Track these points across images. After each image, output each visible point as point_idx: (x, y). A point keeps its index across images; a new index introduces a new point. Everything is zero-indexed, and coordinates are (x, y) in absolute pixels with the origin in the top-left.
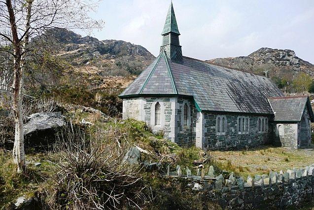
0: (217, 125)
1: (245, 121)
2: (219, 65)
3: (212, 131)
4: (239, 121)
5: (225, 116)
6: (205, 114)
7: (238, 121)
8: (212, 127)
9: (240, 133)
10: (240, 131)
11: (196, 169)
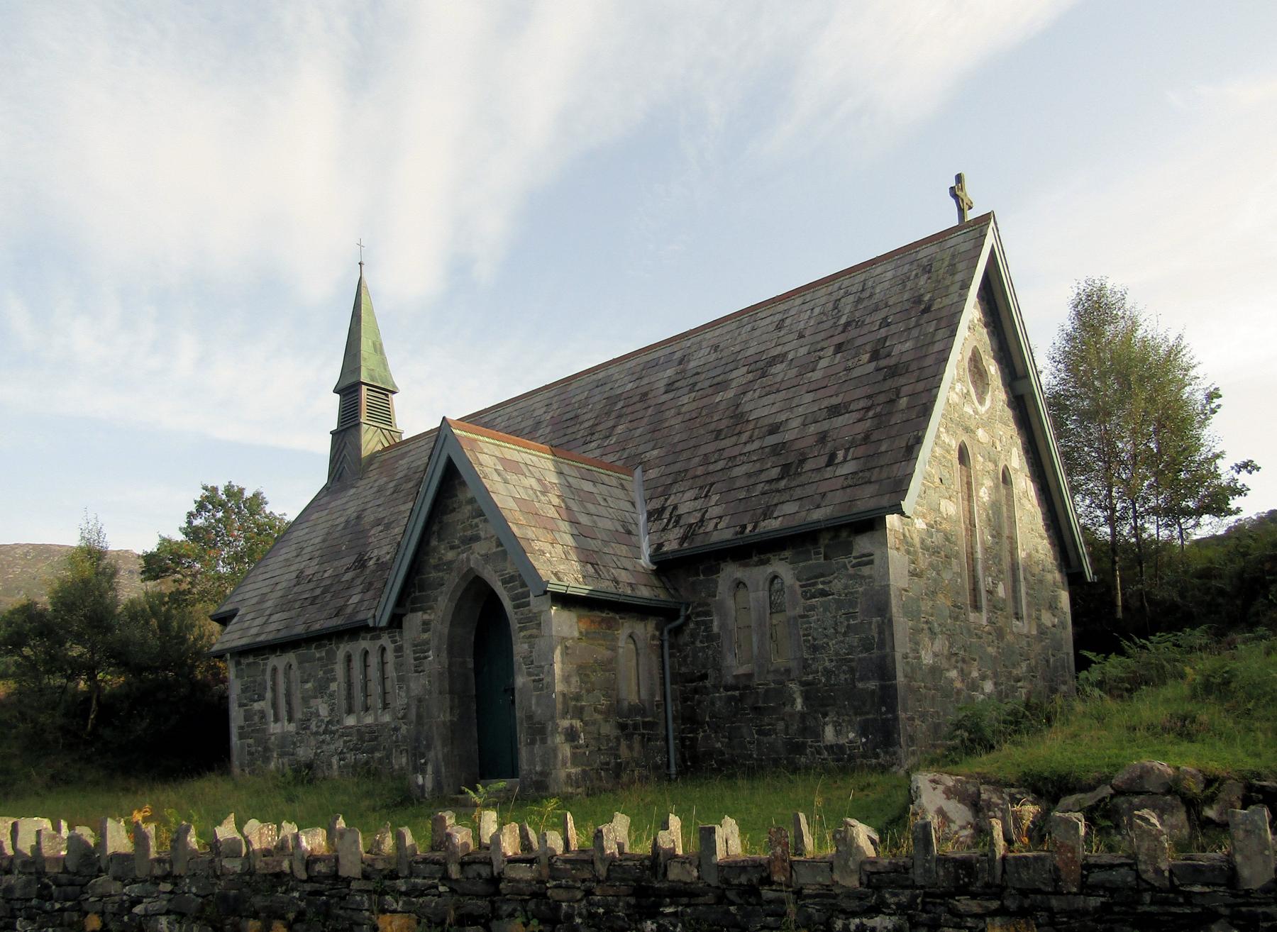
0: (269, 695)
5: (291, 657)
6: (238, 664)
7: (339, 669)
10: (350, 711)
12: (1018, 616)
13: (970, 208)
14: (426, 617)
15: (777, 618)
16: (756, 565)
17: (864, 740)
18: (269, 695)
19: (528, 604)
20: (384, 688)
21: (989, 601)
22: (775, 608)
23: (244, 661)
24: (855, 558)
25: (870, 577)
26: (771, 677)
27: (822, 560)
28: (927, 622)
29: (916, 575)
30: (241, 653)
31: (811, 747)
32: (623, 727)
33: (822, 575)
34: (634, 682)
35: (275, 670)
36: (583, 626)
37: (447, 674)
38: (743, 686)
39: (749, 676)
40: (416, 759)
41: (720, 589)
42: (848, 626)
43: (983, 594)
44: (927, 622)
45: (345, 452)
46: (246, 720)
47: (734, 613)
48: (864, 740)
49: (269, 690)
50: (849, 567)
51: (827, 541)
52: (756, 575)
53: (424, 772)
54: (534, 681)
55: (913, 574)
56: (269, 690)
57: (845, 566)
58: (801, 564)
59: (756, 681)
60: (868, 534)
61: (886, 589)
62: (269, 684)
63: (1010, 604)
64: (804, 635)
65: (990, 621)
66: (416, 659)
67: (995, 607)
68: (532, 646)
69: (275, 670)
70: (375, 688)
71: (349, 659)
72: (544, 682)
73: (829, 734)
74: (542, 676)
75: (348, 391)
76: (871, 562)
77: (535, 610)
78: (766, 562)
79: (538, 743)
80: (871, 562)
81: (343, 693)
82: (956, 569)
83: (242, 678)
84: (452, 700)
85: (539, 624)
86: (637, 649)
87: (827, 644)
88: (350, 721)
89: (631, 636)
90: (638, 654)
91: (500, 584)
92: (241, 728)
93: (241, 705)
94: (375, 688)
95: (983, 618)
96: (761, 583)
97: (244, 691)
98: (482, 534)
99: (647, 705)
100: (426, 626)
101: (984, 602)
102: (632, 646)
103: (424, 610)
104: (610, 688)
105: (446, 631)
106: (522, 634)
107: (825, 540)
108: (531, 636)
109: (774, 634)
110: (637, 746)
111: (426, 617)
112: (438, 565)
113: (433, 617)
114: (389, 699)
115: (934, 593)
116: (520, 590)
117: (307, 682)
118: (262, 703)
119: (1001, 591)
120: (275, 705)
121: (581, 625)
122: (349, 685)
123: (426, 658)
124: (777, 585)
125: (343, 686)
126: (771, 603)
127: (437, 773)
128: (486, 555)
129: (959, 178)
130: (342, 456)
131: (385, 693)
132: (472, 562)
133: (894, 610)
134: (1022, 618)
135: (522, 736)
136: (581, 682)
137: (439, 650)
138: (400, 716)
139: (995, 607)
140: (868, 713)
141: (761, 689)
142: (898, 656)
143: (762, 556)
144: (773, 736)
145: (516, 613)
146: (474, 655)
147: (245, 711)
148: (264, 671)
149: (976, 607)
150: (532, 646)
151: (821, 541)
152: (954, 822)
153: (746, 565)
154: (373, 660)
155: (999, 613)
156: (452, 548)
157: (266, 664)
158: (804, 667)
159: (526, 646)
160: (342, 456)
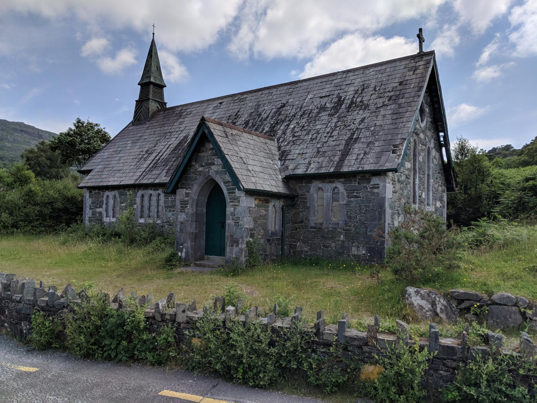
0: (104, 206)
1: (154, 198)
2: (136, 115)
3: (98, 215)
4: (142, 200)
5: (116, 192)
6: (90, 192)
7: (138, 200)
8: (98, 210)
9: (142, 221)
10: (142, 217)
11: (396, 150)
12: (428, 205)
13: (424, 42)
14: (187, 191)
15: (335, 203)
16: (328, 183)
17: (369, 254)
18: (104, 206)
19: (235, 193)
20: (158, 210)
21: (419, 200)
22: (335, 199)
23: (93, 192)
24: (371, 185)
25: (377, 193)
26: (330, 226)
27: (357, 184)
28: (397, 210)
29: (395, 192)
30: (91, 189)
31: (346, 254)
32: (268, 240)
33: (357, 190)
34: (273, 223)
35: (108, 196)
36: (257, 202)
37: (195, 215)
38: (319, 228)
39: (322, 224)
40: (178, 246)
41: (312, 190)
42: (366, 210)
43: (417, 197)
44: (397, 210)
45: (141, 109)
46: (92, 215)
47: (316, 200)
48: (369, 254)
49: (104, 204)
50: (368, 188)
51: (360, 177)
52: (328, 187)
53: (182, 252)
54: (235, 222)
55: (394, 192)
56: (104, 204)
57: (366, 188)
58: (348, 185)
59: (324, 226)
60: (378, 176)
61: (384, 199)
62: (105, 202)
63: (426, 200)
64: (346, 212)
65: (419, 208)
66: (181, 207)
67: (421, 202)
68: (235, 209)
69: (108, 196)
70: (154, 209)
71: (143, 196)
72: (240, 223)
73: (354, 251)
74: (238, 221)
75: (145, 85)
76: (378, 187)
77: (238, 195)
78: (333, 182)
79: (235, 246)
80: (378, 187)
81: (139, 210)
82: (409, 189)
83: (92, 198)
84: (196, 225)
85: (239, 201)
86: (275, 210)
87: (356, 216)
88: (142, 221)
89: (274, 206)
90: (276, 213)
91: (223, 183)
92: (89, 217)
93: (90, 209)
94: (154, 209)
95: (417, 206)
96: (330, 190)
97: (92, 203)
98: (216, 163)
99: (278, 232)
100: (187, 195)
101: (417, 201)
102: (274, 209)
103: (187, 189)
104: (265, 228)
105: (196, 198)
106: (231, 204)
107: (358, 177)
108: (235, 205)
109: (333, 210)
110: (273, 248)
111: (187, 191)
112: (195, 172)
113: (190, 192)
114: (160, 214)
115: (400, 199)
116: (231, 187)
117: (122, 203)
118: (101, 209)
119: (423, 196)
120: (107, 210)
121: (256, 202)
122: (142, 206)
123: (186, 207)
124: (336, 191)
125: (140, 207)
126: (333, 197)
127: (187, 253)
128: (217, 171)
129: (421, 30)
130: (140, 111)
131: (158, 212)
132: (210, 173)
133: (387, 206)
134: (430, 205)
135: (228, 243)
136: (254, 224)
137: (192, 205)
138: (165, 221)
139: (421, 202)
140: (371, 244)
141: (326, 230)
142: (386, 224)
143: (331, 180)
144: (330, 248)
145: (229, 195)
146: (207, 207)
147: (93, 211)
148: (103, 197)
149: (414, 202)
150: (235, 209)
151: (357, 177)
152: (424, 309)
153: (324, 182)
154: (154, 198)
155: (422, 204)
156: (202, 166)
157: (104, 194)
158: (345, 224)
159: (232, 209)
160: (140, 111)
